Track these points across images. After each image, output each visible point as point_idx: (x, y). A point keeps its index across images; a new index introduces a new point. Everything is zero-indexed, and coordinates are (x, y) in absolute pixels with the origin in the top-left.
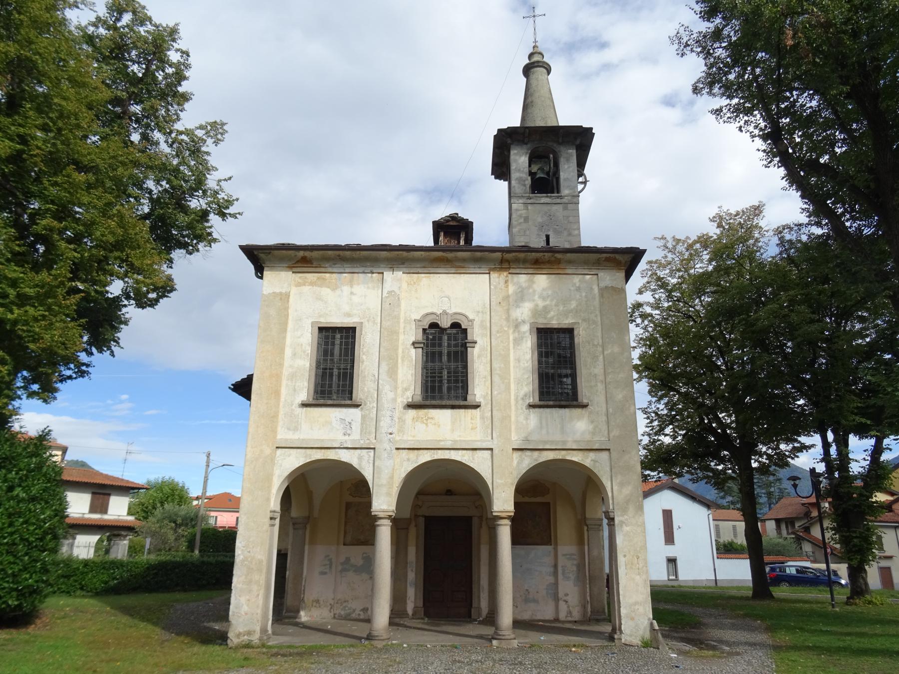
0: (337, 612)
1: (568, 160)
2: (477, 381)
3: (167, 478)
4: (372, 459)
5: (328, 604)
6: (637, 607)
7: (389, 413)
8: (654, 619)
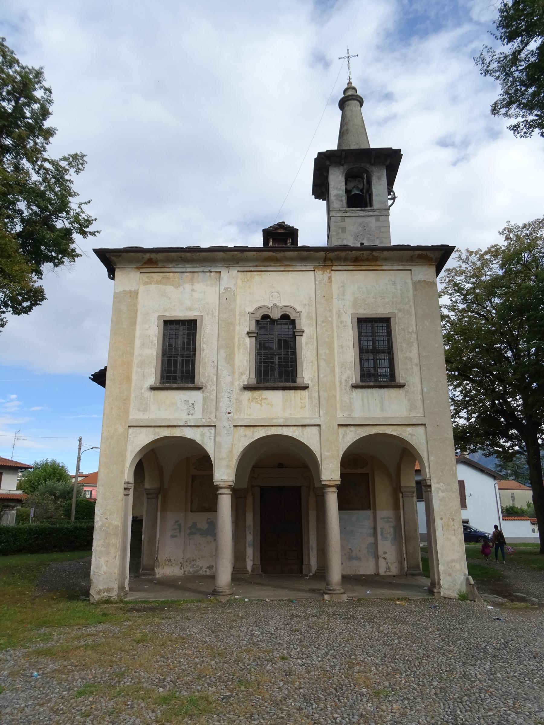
0: (187, 569)
1: (379, 178)
2: (305, 365)
3: (50, 460)
4: (213, 435)
5: (179, 563)
6: (453, 564)
7: (227, 395)
8: (469, 575)
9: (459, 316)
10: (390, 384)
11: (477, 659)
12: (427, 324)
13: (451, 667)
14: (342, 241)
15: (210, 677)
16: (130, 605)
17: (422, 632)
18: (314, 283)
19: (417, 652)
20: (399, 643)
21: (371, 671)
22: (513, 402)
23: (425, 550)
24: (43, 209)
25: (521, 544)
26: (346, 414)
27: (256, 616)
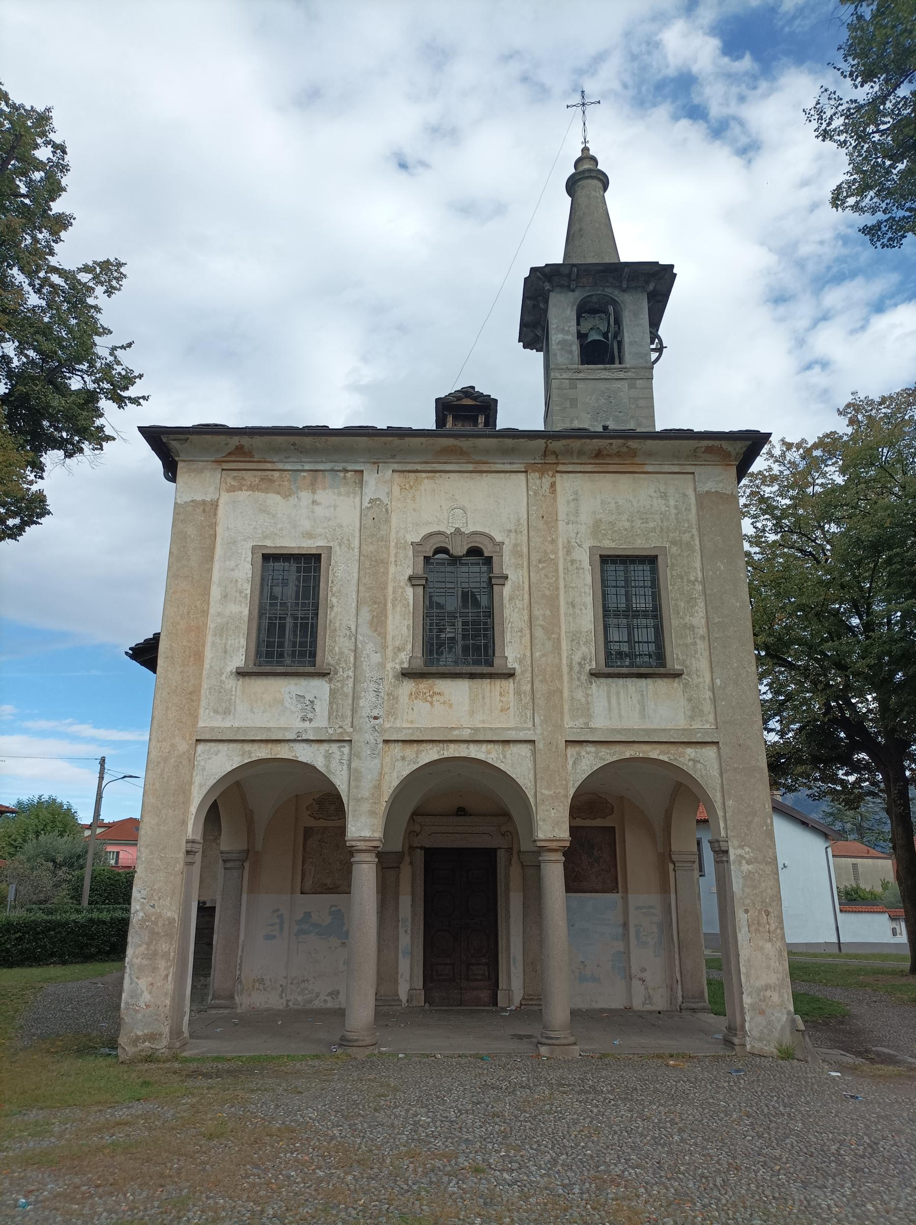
2: (508, 637)
3: (45, 798)
4: (346, 757)
6: (768, 993)
7: (373, 686)
8: (796, 1012)
9: (767, 555)
10: (657, 670)
11: (826, 1175)
12: (722, 567)
13: (783, 1190)
14: (572, 421)
15: (346, 1208)
16: (191, 1065)
17: (721, 1121)
18: (525, 494)
19: (716, 1159)
20: (682, 1140)
21: (638, 1196)
22: (860, 705)
23: (714, 964)
24: (47, 356)
25: (874, 956)
26: (580, 722)
27: (419, 1087)
